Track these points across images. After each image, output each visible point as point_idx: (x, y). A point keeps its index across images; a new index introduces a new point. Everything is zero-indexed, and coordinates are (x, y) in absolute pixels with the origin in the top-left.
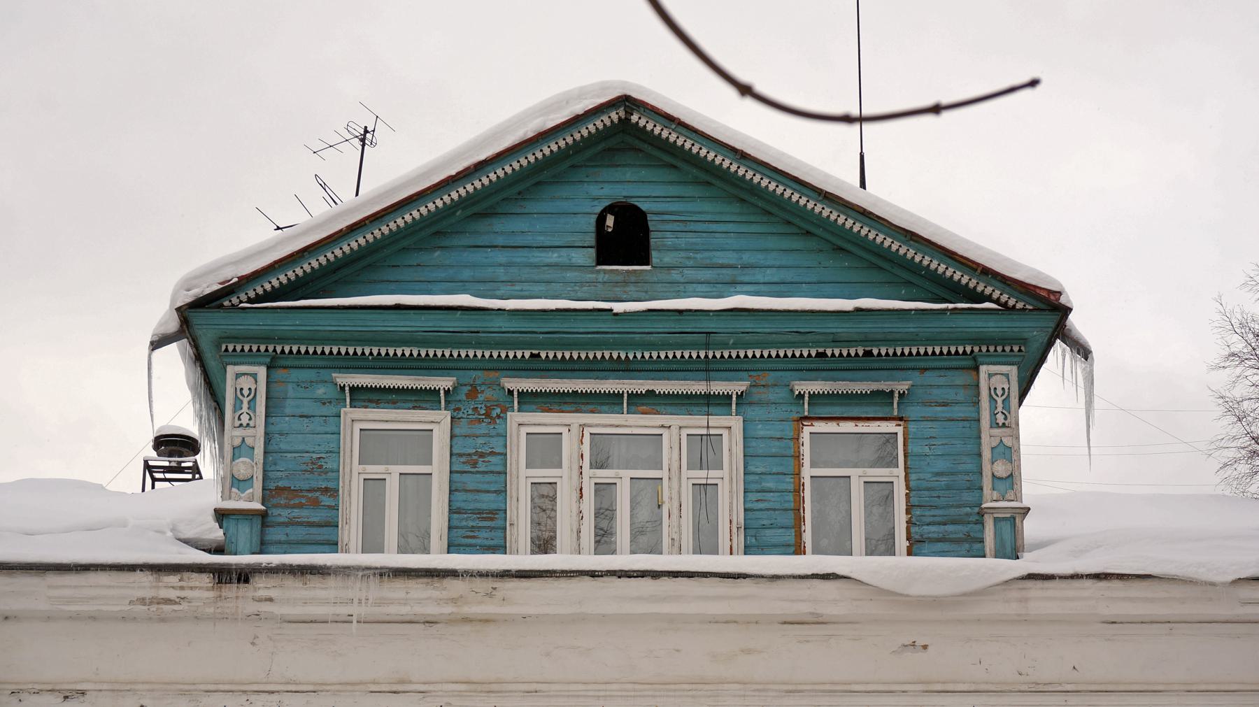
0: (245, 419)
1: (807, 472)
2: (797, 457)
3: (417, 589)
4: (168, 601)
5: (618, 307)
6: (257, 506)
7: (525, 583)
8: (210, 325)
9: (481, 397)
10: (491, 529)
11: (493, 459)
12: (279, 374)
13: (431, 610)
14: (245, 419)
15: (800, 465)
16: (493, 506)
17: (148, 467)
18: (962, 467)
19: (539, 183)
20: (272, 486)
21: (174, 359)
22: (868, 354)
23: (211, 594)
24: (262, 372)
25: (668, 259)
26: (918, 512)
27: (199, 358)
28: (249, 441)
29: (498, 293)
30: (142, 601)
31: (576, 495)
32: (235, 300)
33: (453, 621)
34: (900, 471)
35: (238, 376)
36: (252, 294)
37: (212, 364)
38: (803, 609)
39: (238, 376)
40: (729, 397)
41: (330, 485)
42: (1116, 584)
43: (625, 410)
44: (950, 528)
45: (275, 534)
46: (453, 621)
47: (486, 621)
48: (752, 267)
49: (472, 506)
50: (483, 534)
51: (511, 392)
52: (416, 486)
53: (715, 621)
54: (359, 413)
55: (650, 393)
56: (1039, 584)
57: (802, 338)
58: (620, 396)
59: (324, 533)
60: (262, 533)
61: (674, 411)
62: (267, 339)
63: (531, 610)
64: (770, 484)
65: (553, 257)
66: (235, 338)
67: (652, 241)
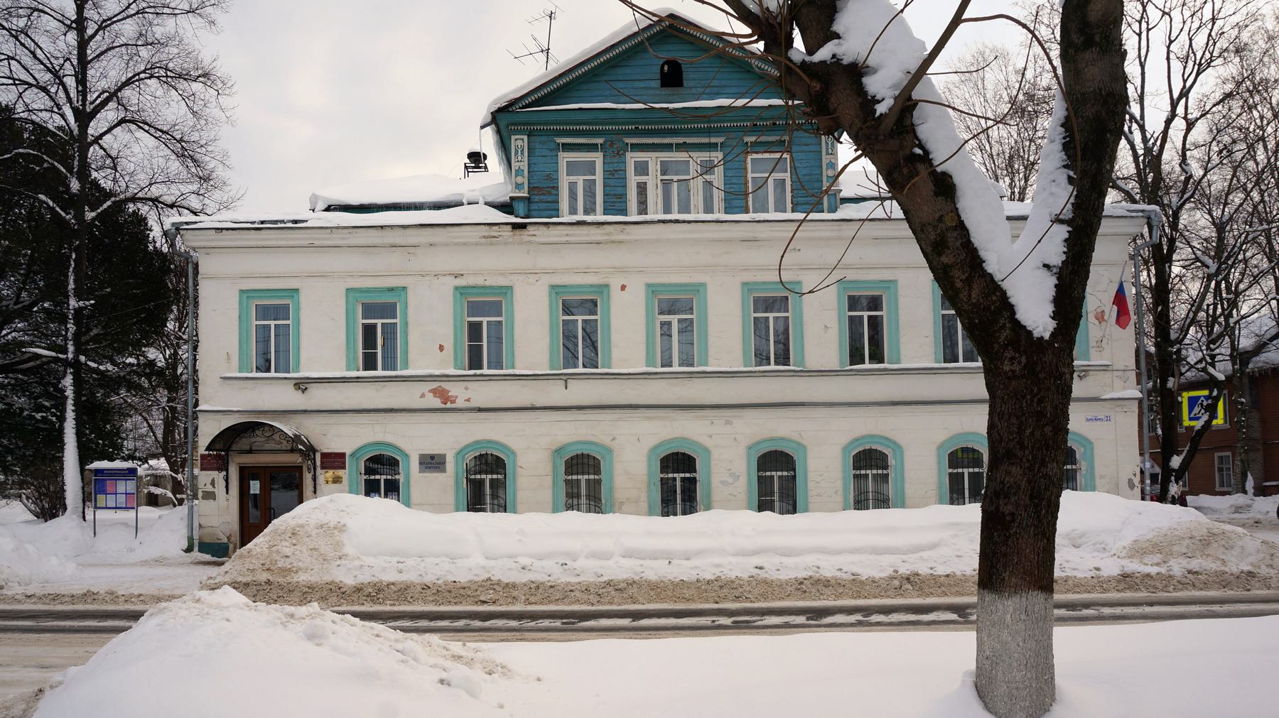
0: (520, 158)
1: (750, 175)
2: (746, 169)
3: (593, 230)
4: (494, 237)
5: (671, 106)
6: (526, 195)
7: (636, 226)
8: (504, 120)
9: (615, 146)
10: (620, 202)
11: (620, 172)
12: (533, 138)
13: (599, 238)
14: (520, 158)
15: (747, 173)
16: (621, 193)
17: (466, 167)
18: (815, 172)
19: (635, 53)
20: (531, 186)
21: (489, 133)
22: (775, 124)
23: (511, 233)
24: (525, 138)
25: (692, 83)
26: (795, 192)
27: (499, 132)
28: (522, 168)
29: (621, 100)
30: (484, 237)
31: (655, 187)
32: (514, 108)
33: (607, 242)
34: (788, 174)
35: (516, 140)
36: (521, 105)
37: (505, 134)
38: (750, 235)
39: (516, 140)
40: (717, 144)
41: (555, 185)
42: (878, 223)
43: (679, 508)
44: (809, 198)
45: (534, 206)
46: (607, 242)
47: (621, 242)
48: (725, 86)
49: (612, 193)
50: (618, 204)
51: (627, 144)
52: (590, 186)
53: (714, 240)
54: (566, 154)
55: (685, 143)
56: (846, 223)
57: (747, 118)
58: (672, 144)
59: (553, 206)
60: (529, 206)
61: (635, 636)
62: (527, 124)
63: (637, 238)
64: (734, 181)
65: (642, 84)
66: (515, 124)
67: (684, 76)
